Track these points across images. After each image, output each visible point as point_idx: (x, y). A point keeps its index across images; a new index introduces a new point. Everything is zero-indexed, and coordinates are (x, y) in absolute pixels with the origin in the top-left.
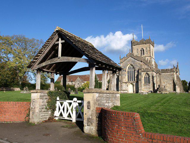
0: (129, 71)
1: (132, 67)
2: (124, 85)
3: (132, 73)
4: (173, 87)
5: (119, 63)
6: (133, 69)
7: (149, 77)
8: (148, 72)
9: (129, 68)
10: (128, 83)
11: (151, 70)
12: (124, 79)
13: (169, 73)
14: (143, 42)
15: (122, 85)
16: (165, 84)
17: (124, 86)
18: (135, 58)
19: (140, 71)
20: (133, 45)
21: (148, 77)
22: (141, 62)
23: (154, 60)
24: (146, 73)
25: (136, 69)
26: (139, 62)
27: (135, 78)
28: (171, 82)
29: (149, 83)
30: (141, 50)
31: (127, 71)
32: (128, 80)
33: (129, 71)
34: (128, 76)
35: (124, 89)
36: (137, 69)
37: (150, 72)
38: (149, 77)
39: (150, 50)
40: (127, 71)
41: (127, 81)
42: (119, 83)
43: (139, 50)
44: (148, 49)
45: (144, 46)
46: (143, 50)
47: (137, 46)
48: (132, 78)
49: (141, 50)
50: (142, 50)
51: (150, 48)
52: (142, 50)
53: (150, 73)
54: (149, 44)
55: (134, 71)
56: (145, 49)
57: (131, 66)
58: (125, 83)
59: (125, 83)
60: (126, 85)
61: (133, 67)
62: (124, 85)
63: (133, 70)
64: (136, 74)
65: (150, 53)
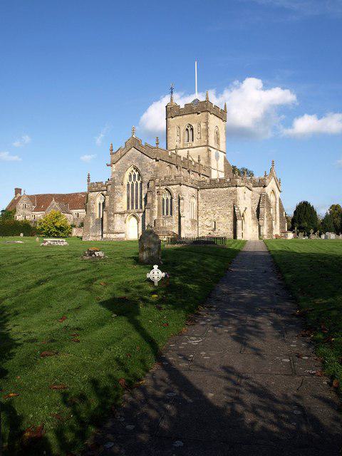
0: (130, 183)
1: (137, 174)
2: (118, 219)
3: (137, 190)
4: (232, 223)
5: (109, 163)
6: (139, 179)
7: (172, 198)
8: (170, 187)
9: (130, 176)
10: (126, 215)
11: (175, 182)
12: (118, 205)
13: (225, 189)
14: (192, 108)
15: (112, 218)
16: (216, 216)
17: (118, 222)
18: (143, 150)
19: (151, 184)
20: (169, 115)
21: (169, 198)
22: (157, 161)
23: (222, 155)
24: (167, 190)
25: (145, 180)
26: (151, 161)
27: (141, 202)
28: (229, 212)
29: (171, 214)
30: (187, 130)
31: (125, 183)
32: (128, 208)
33: (130, 183)
34: (128, 198)
35: (117, 229)
36: (146, 178)
37: (174, 187)
38: (172, 198)
39: (207, 130)
40: (125, 183)
41: (125, 208)
42: (239, 222)
43: (183, 129)
44: (203, 126)
45: (194, 119)
46: (192, 129)
47: (178, 118)
48: (132, 202)
49: (187, 130)
50: (189, 129)
51: (207, 123)
52: (189, 129)
53: (173, 188)
54: (205, 114)
55: (141, 184)
56: (195, 126)
57: (134, 171)
58: (120, 213)
59: (120, 213)
60: (123, 218)
61: (139, 175)
62: (118, 219)
63: (139, 182)
64: (145, 190)
65: (207, 136)
